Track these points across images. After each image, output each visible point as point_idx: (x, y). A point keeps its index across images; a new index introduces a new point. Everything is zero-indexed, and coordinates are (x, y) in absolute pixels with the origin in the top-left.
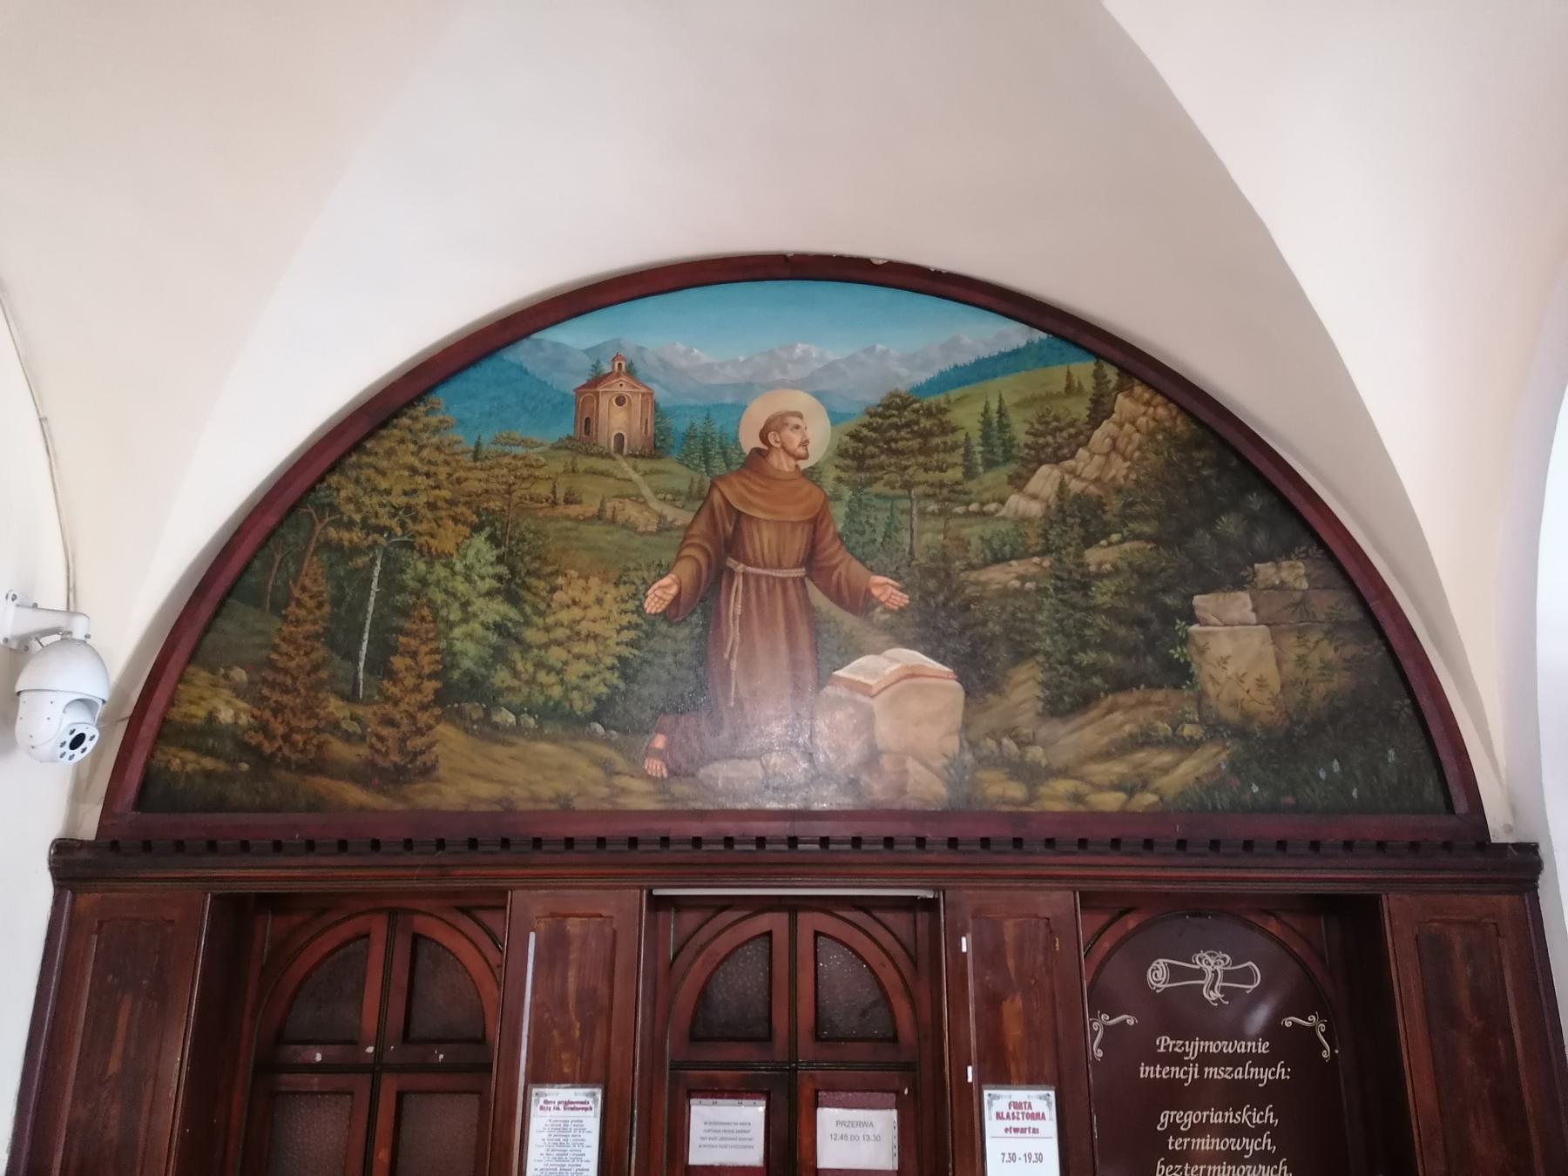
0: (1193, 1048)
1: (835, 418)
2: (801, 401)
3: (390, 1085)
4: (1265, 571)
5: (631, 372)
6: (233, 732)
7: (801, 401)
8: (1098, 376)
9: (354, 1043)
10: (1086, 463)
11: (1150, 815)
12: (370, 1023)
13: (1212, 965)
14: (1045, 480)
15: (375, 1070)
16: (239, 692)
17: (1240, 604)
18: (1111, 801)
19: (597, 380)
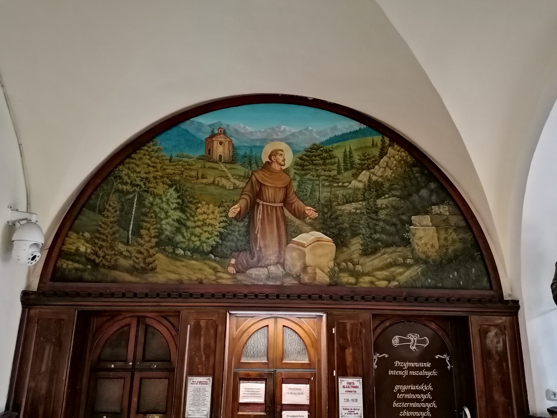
0: (406, 365)
1: (294, 152)
2: (283, 145)
3: (137, 376)
6: (85, 255)
9: (126, 361)
10: (378, 170)
11: (400, 287)
12: (130, 356)
13: (413, 338)
14: (364, 176)
15: (133, 370)
17: (426, 219)
18: (383, 284)
19: (213, 136)
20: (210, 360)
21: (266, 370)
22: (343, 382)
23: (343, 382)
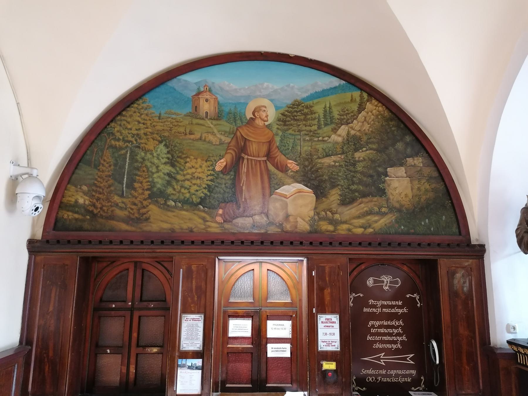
0: (379, 303)
1: (277, 108)
2: (266, 102)
3: (136, 314)
4: (410, 160)
5: (210, 91)
6: (84, 206)
7: (266, 102)
8: (361, 96)
10: (356, 125)
11: (375, 233)
12: (130, 296)
13: (386, 279)
14: (343, 130)
15: (132, 310)
16: (85, 193)
17: (401, 171)
18: (360, 231)
19: (199, 93)
20: (202, 299)
21: (252, 309)
22: (322, 318)
23: (322, 318)
